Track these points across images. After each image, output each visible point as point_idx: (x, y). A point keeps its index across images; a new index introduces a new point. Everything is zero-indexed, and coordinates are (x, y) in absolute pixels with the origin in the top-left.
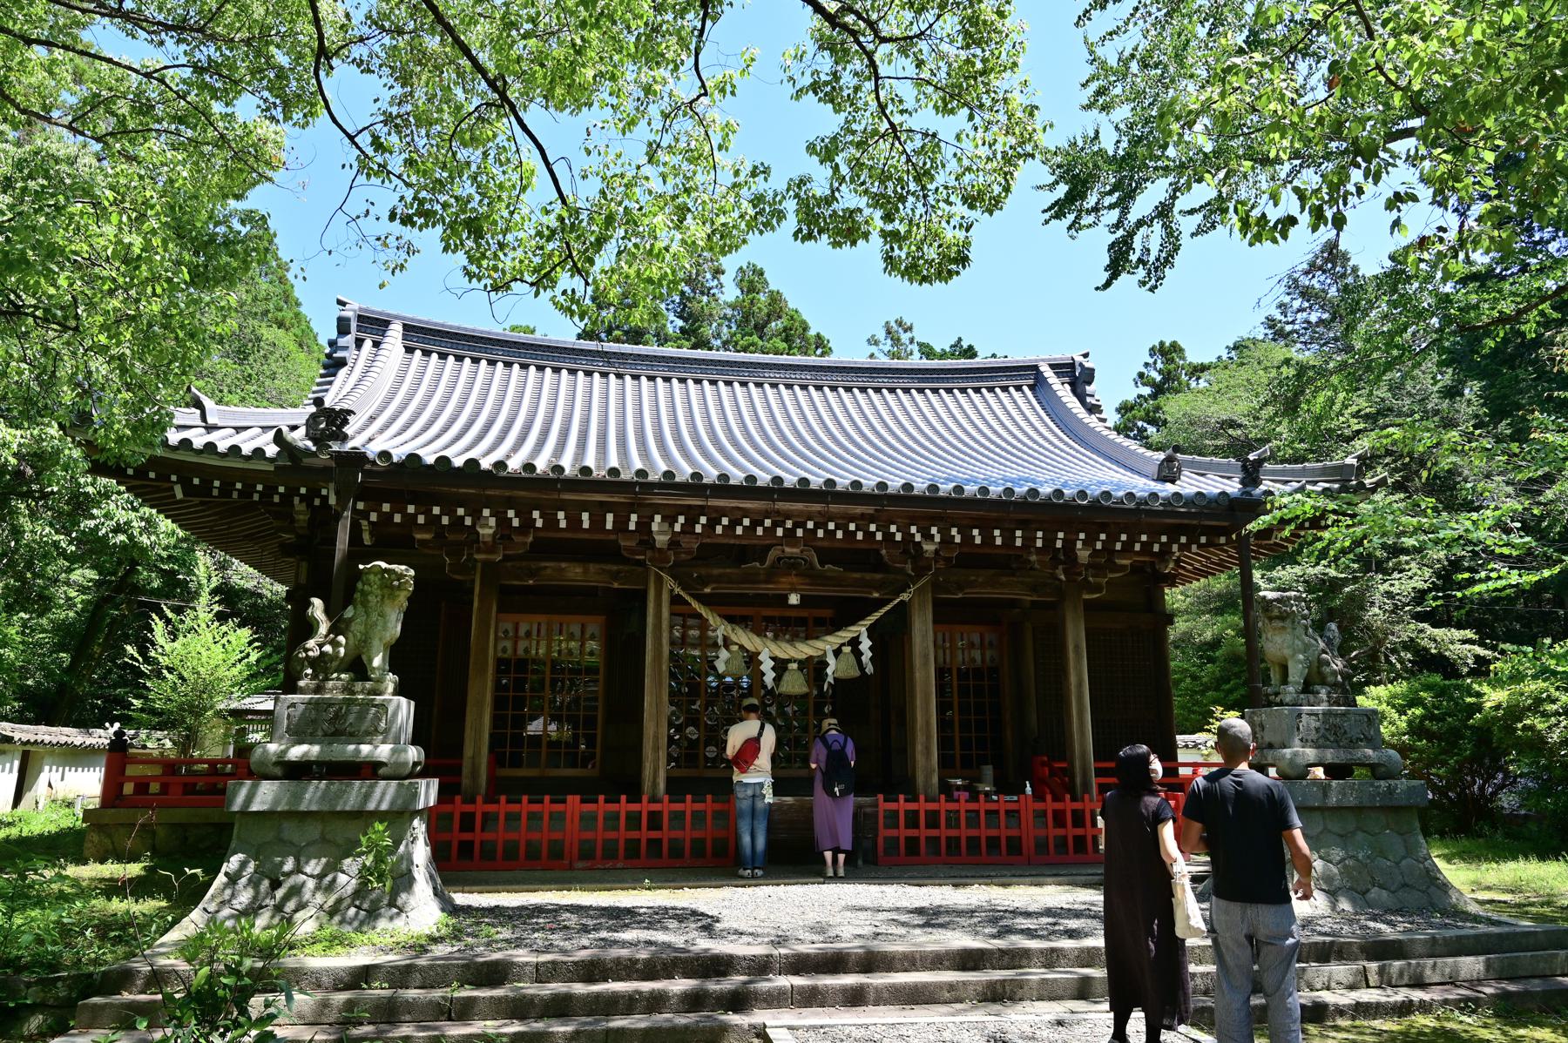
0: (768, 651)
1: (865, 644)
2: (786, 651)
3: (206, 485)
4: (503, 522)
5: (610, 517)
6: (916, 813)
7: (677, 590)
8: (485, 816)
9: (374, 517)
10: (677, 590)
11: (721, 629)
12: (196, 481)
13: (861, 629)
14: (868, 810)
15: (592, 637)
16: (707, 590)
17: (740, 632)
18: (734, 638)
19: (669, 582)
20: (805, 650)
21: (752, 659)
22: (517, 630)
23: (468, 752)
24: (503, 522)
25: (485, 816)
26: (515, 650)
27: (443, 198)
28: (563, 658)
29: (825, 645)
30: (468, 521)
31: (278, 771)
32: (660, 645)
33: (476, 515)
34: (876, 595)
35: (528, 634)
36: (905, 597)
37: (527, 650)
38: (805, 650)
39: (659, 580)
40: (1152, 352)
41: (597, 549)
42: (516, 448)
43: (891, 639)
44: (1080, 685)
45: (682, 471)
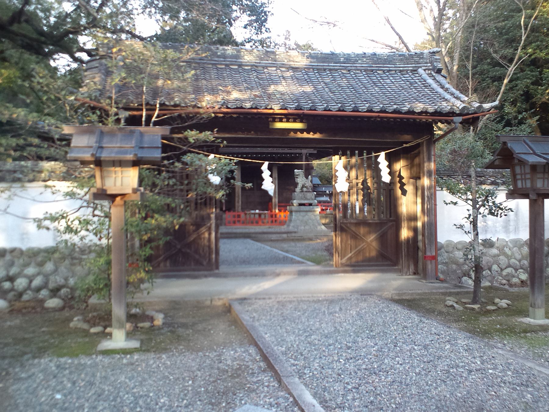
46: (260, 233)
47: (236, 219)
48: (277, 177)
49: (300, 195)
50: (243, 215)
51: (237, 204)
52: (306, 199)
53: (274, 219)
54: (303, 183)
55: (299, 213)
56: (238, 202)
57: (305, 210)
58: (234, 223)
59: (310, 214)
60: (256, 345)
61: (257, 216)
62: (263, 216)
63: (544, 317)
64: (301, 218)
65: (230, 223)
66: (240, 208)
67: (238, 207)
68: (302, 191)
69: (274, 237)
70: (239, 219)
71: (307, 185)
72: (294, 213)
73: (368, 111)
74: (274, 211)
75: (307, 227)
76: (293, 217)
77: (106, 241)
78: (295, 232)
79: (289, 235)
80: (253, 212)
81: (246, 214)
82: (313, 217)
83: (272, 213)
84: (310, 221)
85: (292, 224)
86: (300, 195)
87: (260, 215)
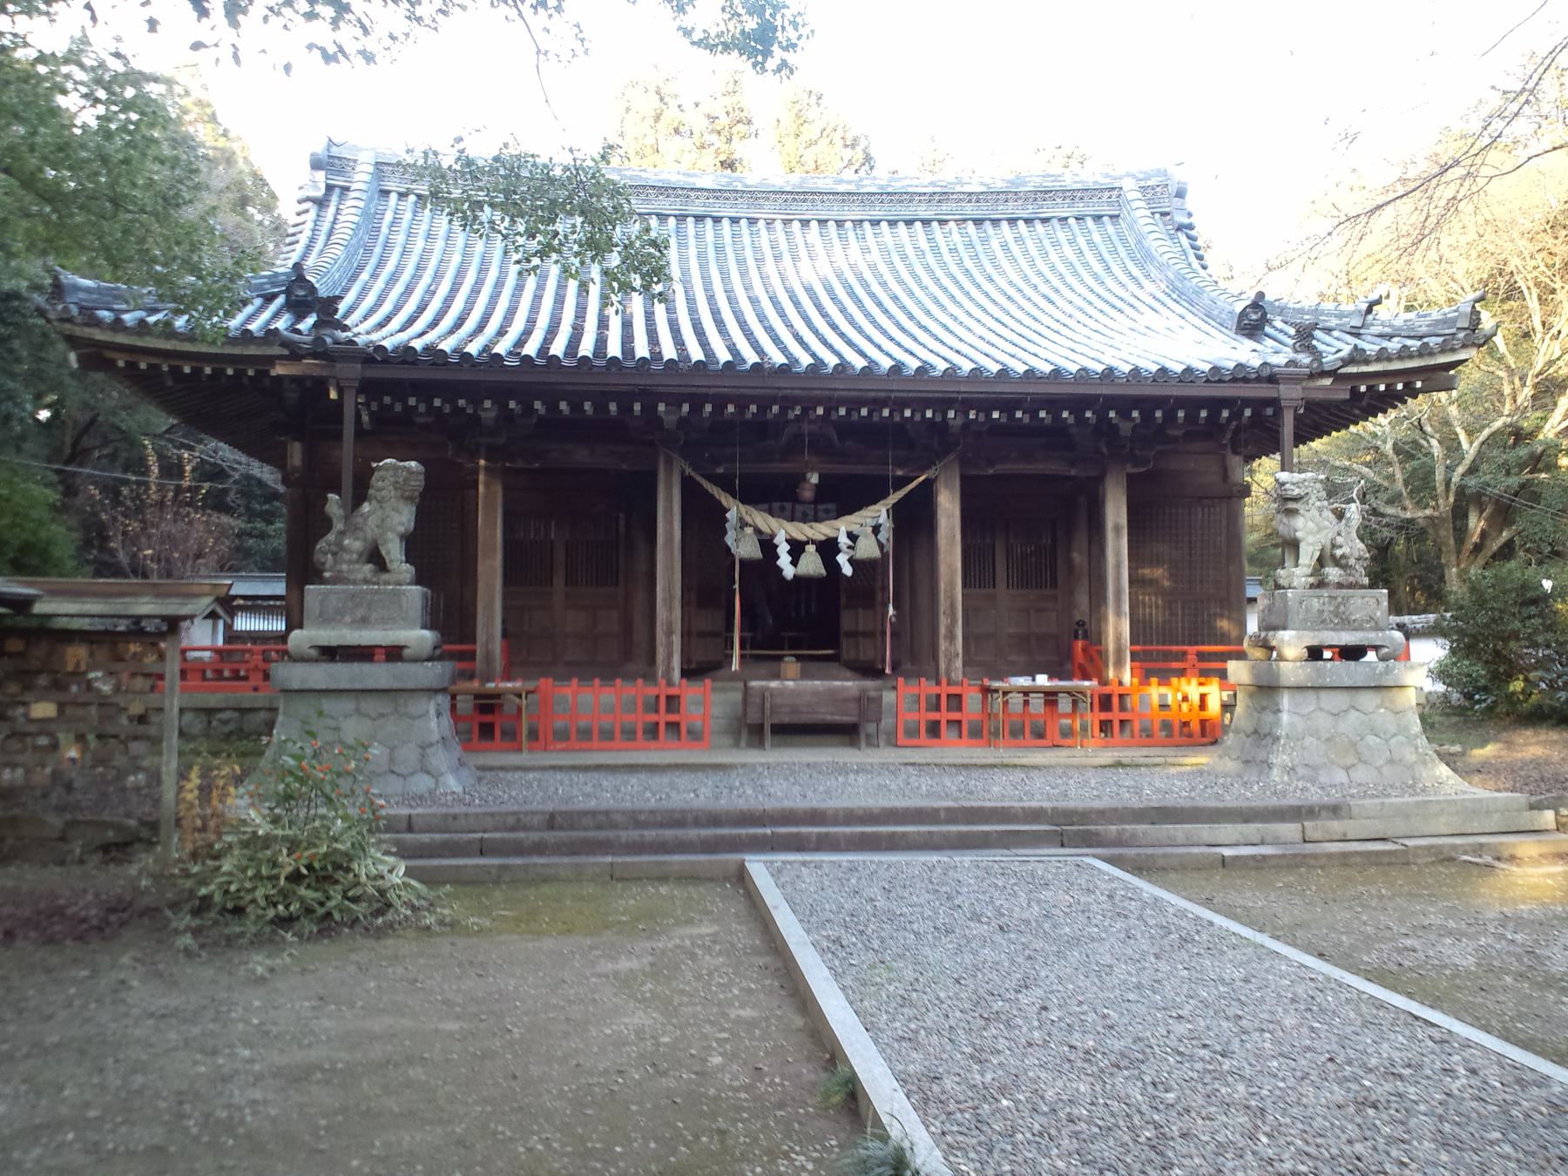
0: (784, 532)
2: (802, 531)
6: (669, 711)
7: (689, 471)
8: (938, 708)
9: (374, 406)
10: (689, 471)
11: (735, 510)
16: (720, 470)
18: (748, 519)
20: (821, 531)
21: (768, 546)
23: (481, 636)
25: (938, 708)
29: (840, 528)
31: (313, 652)
32: (672, 529)
33: (477, 403)
38: (821, 531)
42: (501, 332)
43: (914, 522)
44: (1118, 566)
45: (744, 361)
46: (1141, 815)
47: (944, 716)
48: (1124, 521)
49: (1316, 604)
50: (972, 700)
51: (943, 645)
52: (1346, 624)
53: (1115, 715)
54: (1324, 538)
55: (1311, 696)
56: (951, 637)
57: (384, 683)
58: (934, 730)
59: (1368, 700)
60: (745, 888)
61: (1037, 703)
62: (1064, 704)
63: (419, 622)
64: (1323, 721)
65: (913, 732)
66: (959, 663)
67: (950, 661)
68: (1321, 584)
69: (1232, 840)
70: (955, 716)
71: (1345, 550)
72: (1286, 700)
73: (1287, 365)
74: (1111, 674)
75: (1362, 774)
76: (1285, 717)
77: (580, 698)
78: (1335, 810)
79: (1313, 828)
80: (1023, 681)
81: (986, 691)
82: (1383, 717)
83: (1107, 690)
84: (1371, 739)
85: (1280, 758)
86: (1316, 604)
87: (1051, 697)
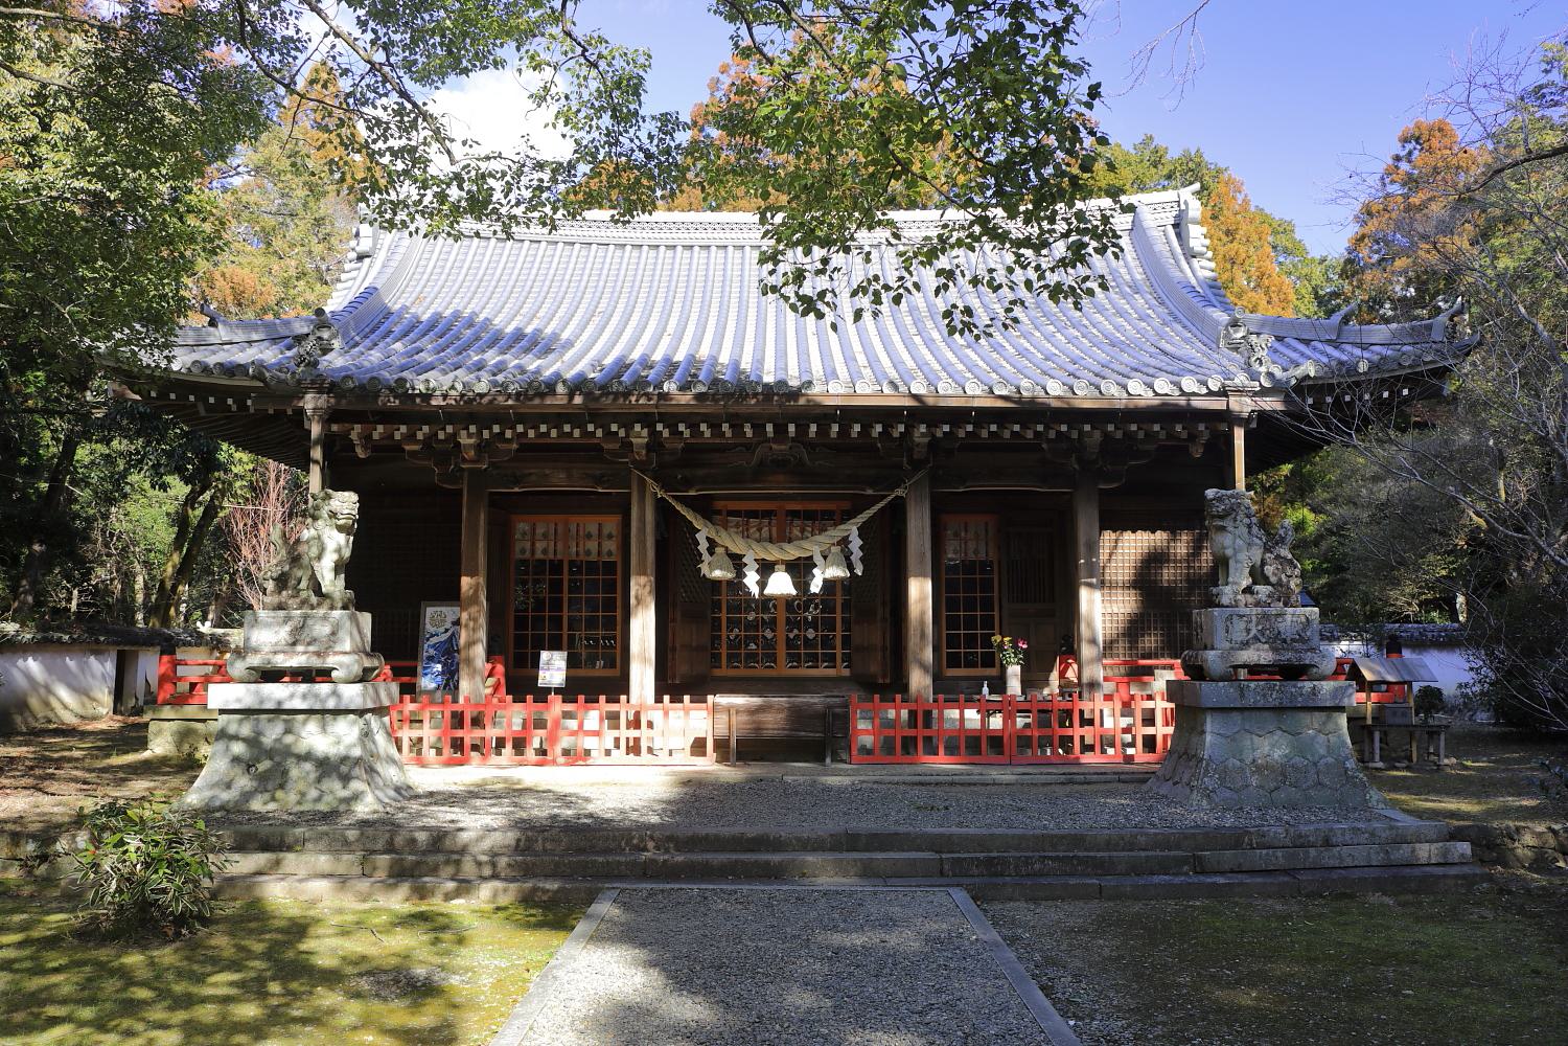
1: (856, 543)
3: (221, 401)
4: (653, 434)
5: (813, 428)
12: (212, 400)
13: (852, 529)
14: (838, 710)
15: (610, 537)
17: (723, 534)
19: (654, 488)
22: (534, 530)
24: (653, 434)
26: (533, 552)
27: (274, 9)
28: (581, 558)
30: (622, 433)
34: (870, 492)
35: (545, 536)
36: (899, 492)
37: (545, 551)
39: (642, 484)
40: (1405, 140)
41: (589, 452)
